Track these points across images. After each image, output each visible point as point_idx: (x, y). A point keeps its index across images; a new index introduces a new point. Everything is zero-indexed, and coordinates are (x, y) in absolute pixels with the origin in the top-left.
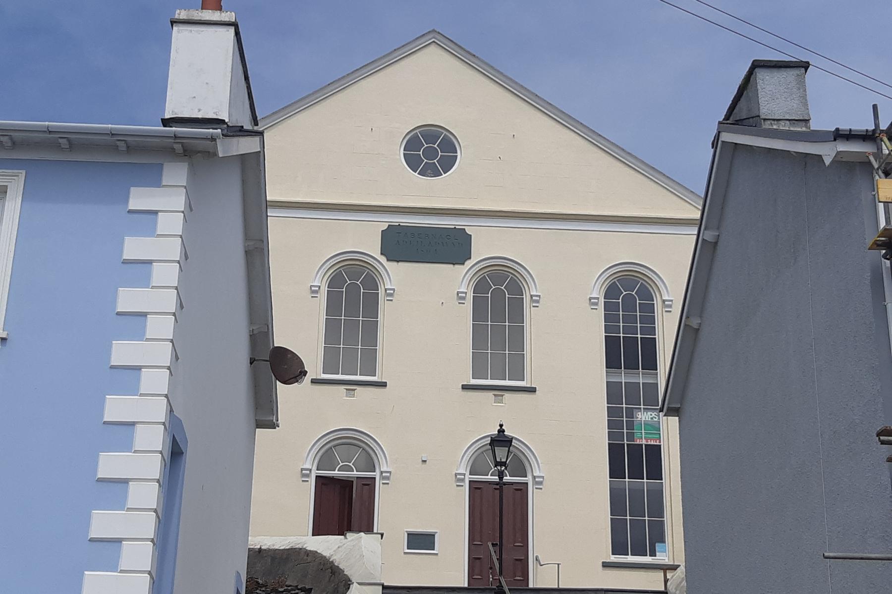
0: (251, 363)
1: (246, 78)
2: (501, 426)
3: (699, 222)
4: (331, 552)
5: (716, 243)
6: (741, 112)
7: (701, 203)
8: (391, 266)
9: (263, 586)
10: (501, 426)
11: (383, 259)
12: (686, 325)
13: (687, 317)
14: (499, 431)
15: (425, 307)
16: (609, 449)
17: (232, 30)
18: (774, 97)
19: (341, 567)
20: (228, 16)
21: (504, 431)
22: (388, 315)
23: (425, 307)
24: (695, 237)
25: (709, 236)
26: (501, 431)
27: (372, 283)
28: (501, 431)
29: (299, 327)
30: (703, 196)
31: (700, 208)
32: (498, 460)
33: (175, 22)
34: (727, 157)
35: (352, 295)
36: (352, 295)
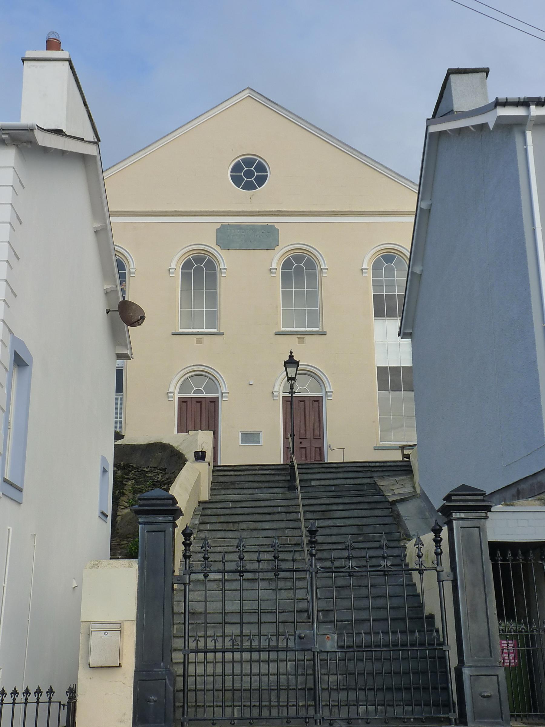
0: (108, 313)
1: (85, 105)
2: (291, 353)
3: (415, 213)
4: (179, 444)
5: (429, 210)
6: (442, 108)
7: (417, 188)
8: (224, 253)
9: (136, 468)
10: (291, 353)
11: (218, 248)
12: (412, 272)
13: (412, 268)
14: (290, 356)
15: (249, 282)
16: (24, 361)
17: (67, 63)
18: (466, 97)
19: (184, 453)
20: (64, 54)
21: (293, 357)
22: (225, 285)
23: (249, 282)
24: (413, 224)
25: (424, 205)
26: (291, 357)
27: (211, 265)
28: (291, 357)
29: (156, 288)
30: (418, 183)
31: (417, 192)
32: (289, 376)
33: (25, 60)
34: (434, 141)
35: (199, 271)
36: (199, 271)
